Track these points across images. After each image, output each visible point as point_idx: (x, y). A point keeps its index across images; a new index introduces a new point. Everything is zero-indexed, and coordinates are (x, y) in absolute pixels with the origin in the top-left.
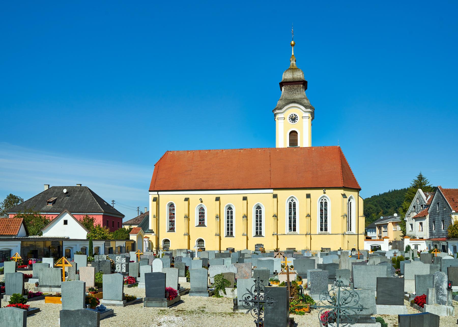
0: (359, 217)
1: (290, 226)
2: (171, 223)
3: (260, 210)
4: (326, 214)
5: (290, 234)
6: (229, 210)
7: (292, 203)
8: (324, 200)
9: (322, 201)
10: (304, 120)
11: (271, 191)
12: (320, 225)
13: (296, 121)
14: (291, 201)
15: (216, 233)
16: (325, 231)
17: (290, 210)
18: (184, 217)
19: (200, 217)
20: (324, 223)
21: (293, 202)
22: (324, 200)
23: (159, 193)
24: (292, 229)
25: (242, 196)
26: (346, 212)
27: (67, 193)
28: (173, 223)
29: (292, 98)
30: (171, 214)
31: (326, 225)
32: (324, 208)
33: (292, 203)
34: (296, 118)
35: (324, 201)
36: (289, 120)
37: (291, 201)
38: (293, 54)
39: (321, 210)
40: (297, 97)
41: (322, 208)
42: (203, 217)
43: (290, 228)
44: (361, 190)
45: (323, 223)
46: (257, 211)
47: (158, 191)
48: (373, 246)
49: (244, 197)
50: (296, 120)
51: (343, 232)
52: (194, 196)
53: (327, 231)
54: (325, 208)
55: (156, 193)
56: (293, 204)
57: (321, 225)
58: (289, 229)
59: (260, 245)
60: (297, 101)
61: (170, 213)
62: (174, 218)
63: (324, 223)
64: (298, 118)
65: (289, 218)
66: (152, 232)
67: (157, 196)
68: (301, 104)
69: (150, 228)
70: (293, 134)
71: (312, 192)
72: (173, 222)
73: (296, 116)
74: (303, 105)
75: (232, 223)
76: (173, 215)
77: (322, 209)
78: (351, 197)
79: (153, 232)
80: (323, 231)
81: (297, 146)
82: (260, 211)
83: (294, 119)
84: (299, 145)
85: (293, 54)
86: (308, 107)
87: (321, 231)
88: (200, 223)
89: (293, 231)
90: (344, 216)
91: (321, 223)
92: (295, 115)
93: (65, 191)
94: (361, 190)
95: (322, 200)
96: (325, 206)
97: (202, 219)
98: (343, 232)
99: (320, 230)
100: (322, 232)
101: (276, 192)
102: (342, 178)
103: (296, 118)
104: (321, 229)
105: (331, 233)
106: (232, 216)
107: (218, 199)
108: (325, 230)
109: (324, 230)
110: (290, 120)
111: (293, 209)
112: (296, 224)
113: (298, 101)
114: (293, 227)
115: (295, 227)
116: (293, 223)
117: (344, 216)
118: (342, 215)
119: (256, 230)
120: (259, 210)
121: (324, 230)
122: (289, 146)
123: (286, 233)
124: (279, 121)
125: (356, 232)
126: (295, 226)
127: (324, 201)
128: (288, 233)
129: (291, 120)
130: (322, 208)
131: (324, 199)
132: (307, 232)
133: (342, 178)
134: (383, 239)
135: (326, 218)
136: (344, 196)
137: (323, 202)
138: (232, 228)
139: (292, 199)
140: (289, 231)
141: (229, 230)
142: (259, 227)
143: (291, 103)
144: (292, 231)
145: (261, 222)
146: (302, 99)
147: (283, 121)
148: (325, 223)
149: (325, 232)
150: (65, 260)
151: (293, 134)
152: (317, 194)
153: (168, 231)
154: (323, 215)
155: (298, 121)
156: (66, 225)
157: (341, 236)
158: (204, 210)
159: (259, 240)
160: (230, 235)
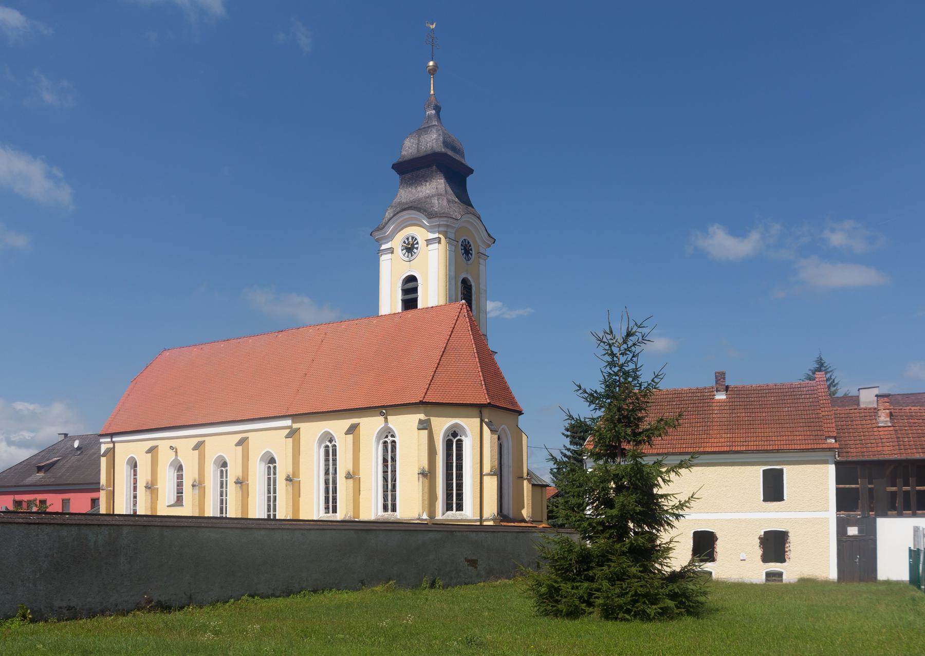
0: (485, 478)
6: (223, 469)
9: (448, 438)
11: (288, 422)
26: (425, 464)
27: (79, 448)
38: (432, 92)
39: (385, 461)
52: (164, 442)
57: (385, 498)
70: (410, 287)
73: (416, 239)
83: (410, 248)
85: (432, 92)
87: (386, 512)
90: (423, 474)
92: (413, 238)
93: (76, 444)
95: (387, 437)
99: (384, 508)
103: (416, 246)
106: (182, 475)
117: (423, 474)
125: (474, 513)
141: (223, 504)
145: (178, 482)
151: (410, 287)
152: (371, 425)
154: (387, 472)
156: (792, 538)
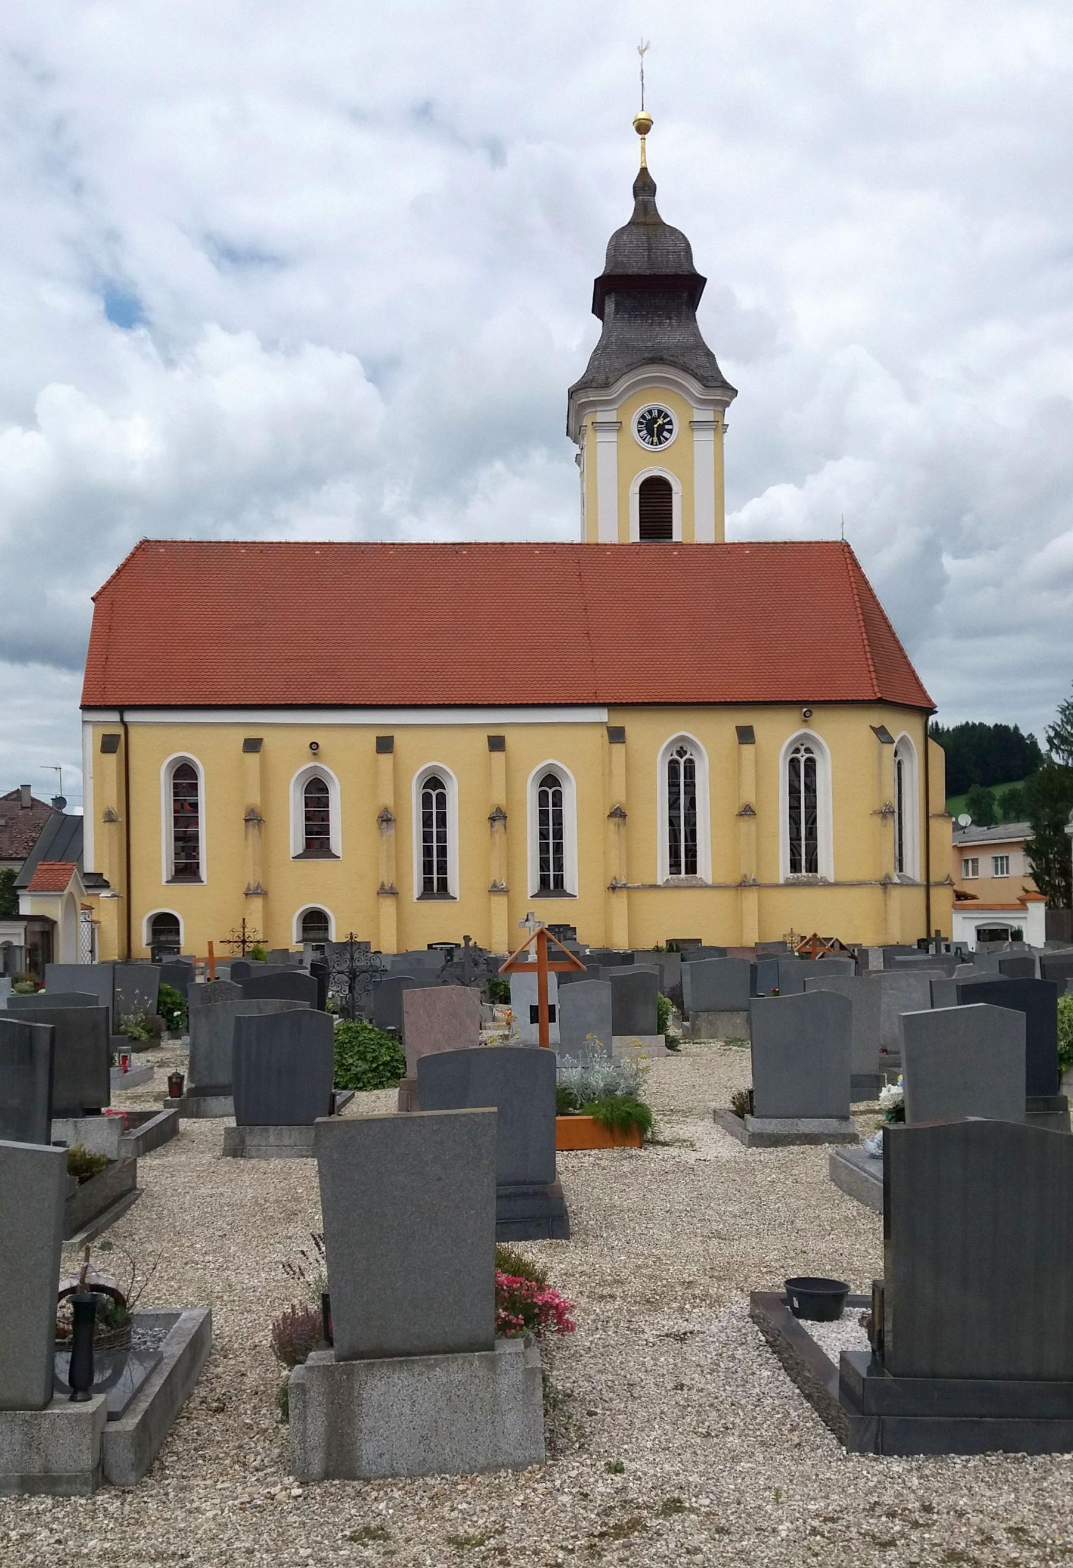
0: (932, 822)
1: (674, 852)
2: (181, 844)
3: (437, 791)
4: (812, 807)
5: (677, 883)
6: (547, 789)
7: (682, 761)
8: (802, 752)
10: (698, 435)
11: (601, 715)
12: (791, 850)
13: (667, 439)
14: (676, 757)
15: (383, 885)
16: (811, 872)
17: (674, 789)
18: (246, 820)
19: (307, 819)
20: (803, 842)
21: (685, 758)
22: (802, 752)
23: (130, 717)
24: (680, 865)
25: (239, 737)
28: (189, 844)
29: (649, 344)
30: (180, 808)
31: (812, 851)
32: (805, 783)
33: (682, 761)
34: (667, 427)
35: (802, 757)
36: (639, 431)
37: (676, 757)
40: (665, 339)
41: (796, 781)
42: (323, 820)
43: (673, 859)
44: (936, 712)
45: (800, 840)
46: (545, 793)
47: (121, 709)
48: (985, 930)
49: (380, 740)
50: (665, 434)
51: (884, 873)
53: (816, 871)
54: (808, 783)
55: (114, 717)
56: (685, 767)
58: (671, 866)
59: (561, 930)
60: (671, 358)
61: (179, 804)
62: (197, 823)
63: (803, 842)
64: (676, 427)
65: (671, 823)
66: (97, 881)
67: (120, 731)
68: (685, 369)
69: (90, 865)
71: (636, 726)
72: (190, 841)
74: (695, 376)
75: (445, 842)
76: (192, 812)
77: (797, 786)
78: (904, 740)
79: (106, 885)
80: (800, 871)
81: (669, 540)
82: (553, 793)
84: (677, 536)
86: (715, 384)
87: (795, 872)
88: (309, 843)
89: (686, 873)
91: (791, 839)
94: (936, 712)
95: (797, 751)
96: (806, 776)
97: (316, 829)
98: (880, 876)
99: (791, 867)
100: (796, 875)
101: (620, 720)
102: (868, 666)
103: (667, 427)
104: (795, 866)
105: (833, 881)
107: (252, 745)
108: (810, 867)
109: (804, 870)
110: (641, 434)
111: (685, 785)
112: (695, 845)
113: (672, 356)
114: (686, 856)
115: (694, 856)
116: (686, 841)
118: (877, 807)
119: (542, 869)
120: (550, 792)
121: (804, 870)
122: (638, 540)
123: (660, 883)
124: (601, 437)
126: (692, 852)
127: (802, 757)
128: (667, 880)
129: (645, 432)
130: (796, 781)
131: (803, 748)
132: (745, 876)
133: (868, 666)
134: (1025, 905)
135: (812, 820)
136: (881, 733)
137: (798, 761)
138: (446, 861)
139: (682, 748)
140: (671, 874)
142: (432, 857)
143: (648, 364)
144: (683, 875)
145: (561, 838)
146: (686, 347)
147: (613, 437)
148: (806, 839)
149: (810, 875)
150: (158, 1113)
153: (170, 878)
155: (673, 438)
157: (878, 891)
158: (325, 790)
159: (552, 911)
160: (438, 890)
